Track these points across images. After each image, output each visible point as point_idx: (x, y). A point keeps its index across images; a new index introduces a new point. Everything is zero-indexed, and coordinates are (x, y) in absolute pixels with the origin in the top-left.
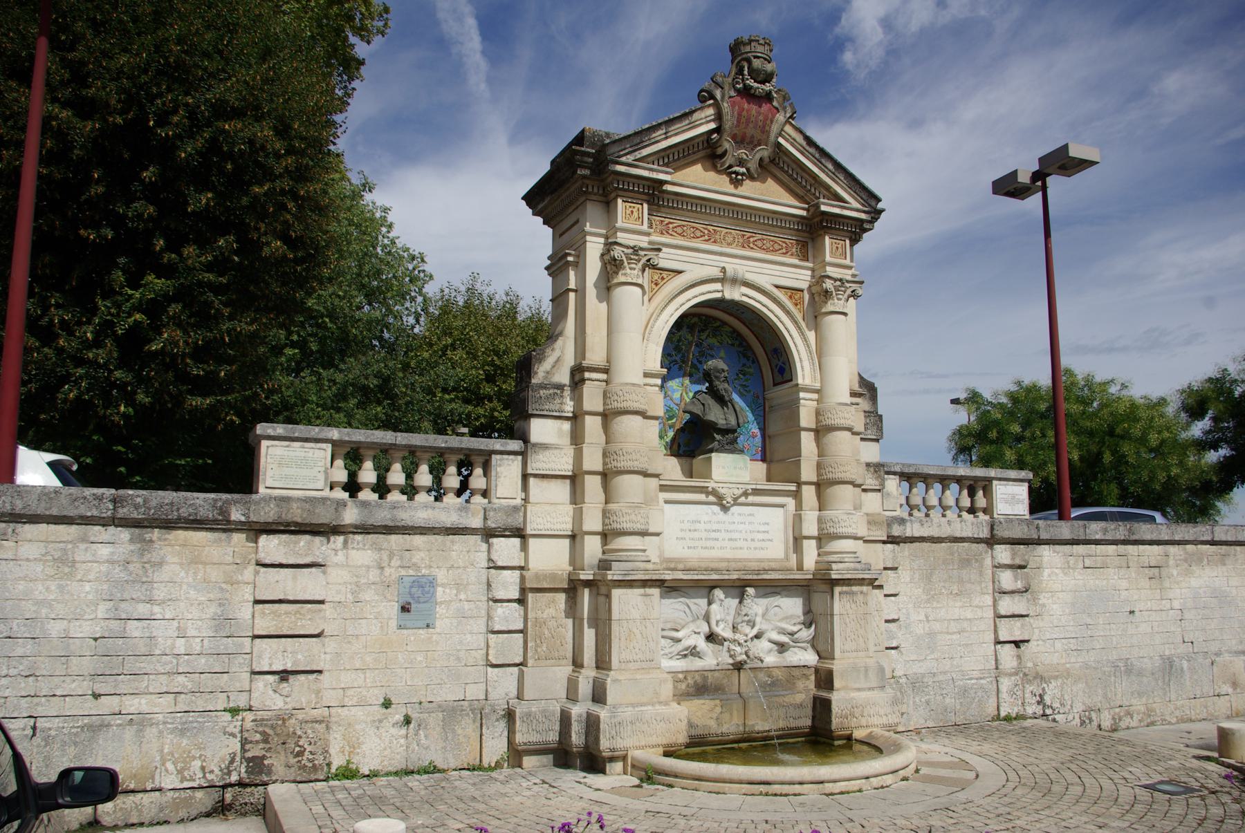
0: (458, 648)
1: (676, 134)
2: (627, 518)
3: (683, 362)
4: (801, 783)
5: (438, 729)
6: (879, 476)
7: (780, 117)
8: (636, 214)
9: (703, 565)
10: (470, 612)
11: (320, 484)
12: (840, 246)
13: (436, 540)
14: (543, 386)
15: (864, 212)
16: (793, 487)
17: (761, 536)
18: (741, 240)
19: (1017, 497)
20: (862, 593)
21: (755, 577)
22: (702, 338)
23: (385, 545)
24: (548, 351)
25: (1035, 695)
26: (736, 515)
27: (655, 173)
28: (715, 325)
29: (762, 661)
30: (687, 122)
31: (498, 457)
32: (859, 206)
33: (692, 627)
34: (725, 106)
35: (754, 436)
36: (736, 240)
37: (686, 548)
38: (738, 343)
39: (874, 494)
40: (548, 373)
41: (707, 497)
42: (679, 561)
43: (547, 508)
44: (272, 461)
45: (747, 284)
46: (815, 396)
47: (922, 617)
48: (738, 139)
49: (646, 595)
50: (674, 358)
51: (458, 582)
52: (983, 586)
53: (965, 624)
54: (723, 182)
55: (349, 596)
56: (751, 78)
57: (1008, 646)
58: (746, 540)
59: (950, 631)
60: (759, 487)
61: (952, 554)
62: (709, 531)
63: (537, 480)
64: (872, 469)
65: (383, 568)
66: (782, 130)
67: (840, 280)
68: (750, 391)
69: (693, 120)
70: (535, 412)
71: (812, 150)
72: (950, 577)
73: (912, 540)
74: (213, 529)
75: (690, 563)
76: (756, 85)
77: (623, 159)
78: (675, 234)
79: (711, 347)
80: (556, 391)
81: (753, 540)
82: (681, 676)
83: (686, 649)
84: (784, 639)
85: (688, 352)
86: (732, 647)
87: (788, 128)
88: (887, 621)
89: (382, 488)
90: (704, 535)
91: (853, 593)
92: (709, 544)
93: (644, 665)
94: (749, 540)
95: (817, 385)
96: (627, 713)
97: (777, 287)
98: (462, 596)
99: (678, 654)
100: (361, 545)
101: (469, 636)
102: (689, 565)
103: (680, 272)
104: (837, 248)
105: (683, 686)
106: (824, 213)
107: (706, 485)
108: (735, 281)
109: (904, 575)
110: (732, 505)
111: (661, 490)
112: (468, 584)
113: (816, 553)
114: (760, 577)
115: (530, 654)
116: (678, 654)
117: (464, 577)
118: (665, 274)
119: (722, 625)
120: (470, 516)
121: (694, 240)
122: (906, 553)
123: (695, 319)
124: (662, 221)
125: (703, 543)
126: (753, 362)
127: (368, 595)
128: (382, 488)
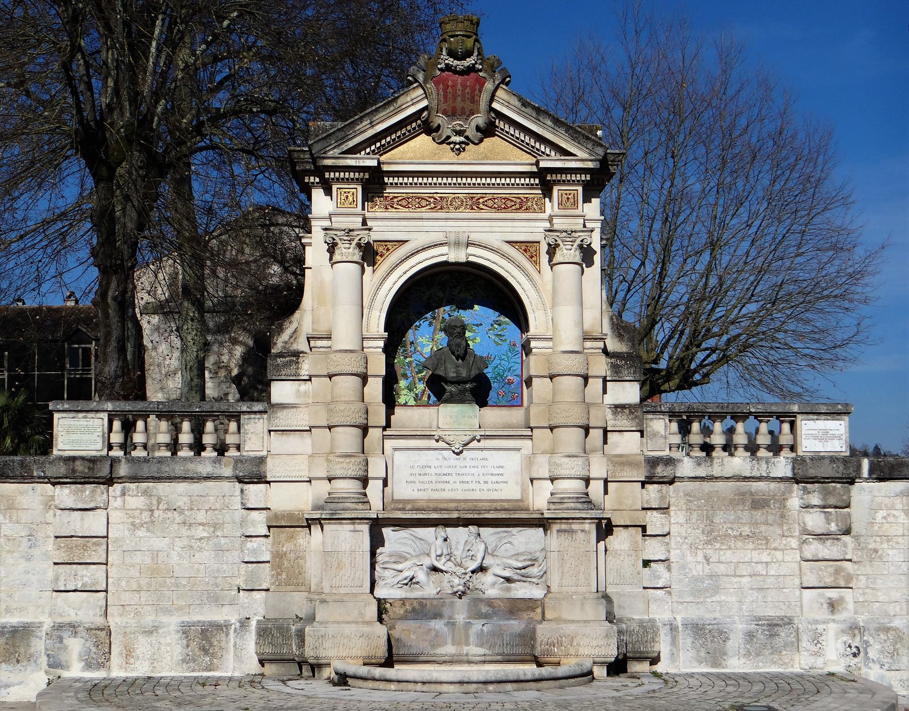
0: (216, 575)
1: (382, 121)
4: (424, 683)
7: (489, 86)
8: (350, 199)
9: (432, 505)
11: (99, 446)
14: (280, 355)
17: (494, 479)
18: (470, 203)
19: (831, 432)
20: (582, 531)
21: (476, 516)
22: (454, 293)
24: (286, 324)
25: (850, 647)
26: (468, 459)
30: (392, 108)
31: (246, 417)
33: (415, 561)
35: (510, 383)
36: (465, 203)
37: (416, 490)
40: (286, 343)
44: (62, 429)
47: (700, 558)
48: (450, 113)
52: (785, 528)
58: (479, 482)
62: (440, 475)
65: (152, 511)
68: (506, 340)
70: (274, 378)
71: (529, 110)
72: (740, 518)
74: (435, 510)
75: (418, 504)
76: (456, 62)
77: (330, 153)
78: (400, 207)
80: (292, 358)
81: (486, 482)
84: (507, 573)
90: (434, 479)
91: (572, 531)
93: (354, 590)
94: (482, 482)
96: (331, 629)
100: (135, 493)
102: (418, 505)
104: (568, 199)
105: (402, 612)
109: (677, 516)
112: (223, 523)
113: (854, 510)
118: (389, 245)
119: (443, 560)
120: (223, 466)
121: (419, 210)
125: (434, 486)
128: (707, 448)
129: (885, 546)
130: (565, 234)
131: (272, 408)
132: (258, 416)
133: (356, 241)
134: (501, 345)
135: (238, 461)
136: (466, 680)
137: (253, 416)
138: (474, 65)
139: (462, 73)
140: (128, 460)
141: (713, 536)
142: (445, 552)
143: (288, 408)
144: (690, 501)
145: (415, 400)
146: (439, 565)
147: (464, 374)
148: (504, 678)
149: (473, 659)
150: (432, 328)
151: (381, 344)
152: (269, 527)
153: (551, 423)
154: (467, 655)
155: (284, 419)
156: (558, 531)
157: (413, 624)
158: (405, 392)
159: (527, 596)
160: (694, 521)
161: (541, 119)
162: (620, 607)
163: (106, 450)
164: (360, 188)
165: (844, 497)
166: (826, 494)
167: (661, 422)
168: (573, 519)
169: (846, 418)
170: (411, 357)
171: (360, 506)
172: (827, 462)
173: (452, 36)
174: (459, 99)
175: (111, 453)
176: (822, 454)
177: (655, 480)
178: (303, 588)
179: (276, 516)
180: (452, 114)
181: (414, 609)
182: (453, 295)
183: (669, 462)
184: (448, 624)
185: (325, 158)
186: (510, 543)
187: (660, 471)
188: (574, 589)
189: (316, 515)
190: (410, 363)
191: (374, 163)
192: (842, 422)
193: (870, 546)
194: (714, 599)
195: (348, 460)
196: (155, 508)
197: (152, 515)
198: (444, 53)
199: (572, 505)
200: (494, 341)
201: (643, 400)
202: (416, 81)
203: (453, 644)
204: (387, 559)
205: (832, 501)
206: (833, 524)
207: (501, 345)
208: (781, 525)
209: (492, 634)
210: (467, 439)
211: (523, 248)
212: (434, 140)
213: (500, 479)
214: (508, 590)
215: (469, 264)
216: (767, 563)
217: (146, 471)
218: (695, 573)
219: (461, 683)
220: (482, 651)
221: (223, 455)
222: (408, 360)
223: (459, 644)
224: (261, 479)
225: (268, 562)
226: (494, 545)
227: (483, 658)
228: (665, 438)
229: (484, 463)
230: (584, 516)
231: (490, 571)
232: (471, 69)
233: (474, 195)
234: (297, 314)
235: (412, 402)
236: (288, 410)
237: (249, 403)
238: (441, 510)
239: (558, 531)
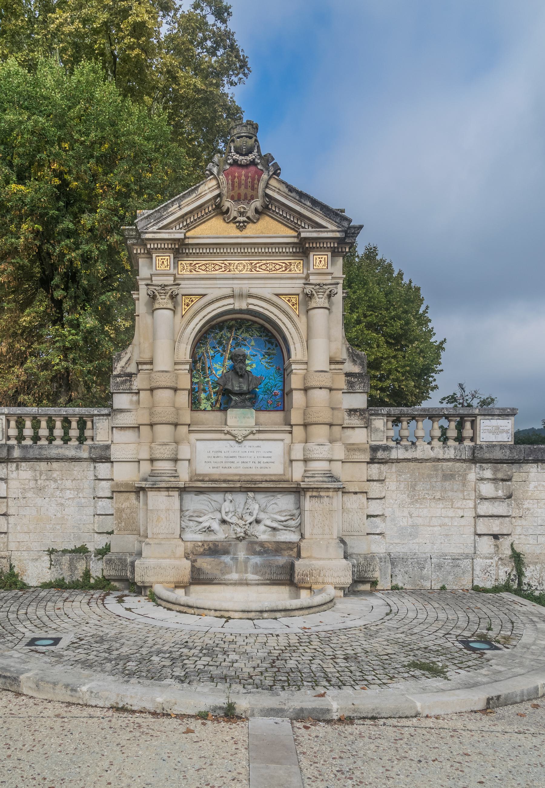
2: (158, 451)
3: (224, 351)
5: (67, 565)
6: (365, 418)
7: (265, 176)
8: (165, 263)
9: (222, 478)
15: (338, 231)
17: (265, 460)
18: (249, 267)
19: (501, 428)
20: (328, 497)
23: (38, 468)
26: (247, 447)
30: (194, 195)
31: (97, 418)
32: (335, 228)
33: (211, 515)
35: (276, 395)
40: (123, 367)
42: (206, 475)
43: (123, 446)
45: (250, 296)
47: (406, 513)
48: (236, 198)
52: (465, 494)
53: (446, 520)
54: (231, 230)
55: (20, 494)
57: (486, 538)
59: (431, 524)
61: (436, 470)
62: (227, 457)
64: (358, 413)
65: (36, 480)
71: (294, 194)
73: (398, 461)
74: (225, 481)
76: (241, 158)
77: (150, 230)
79: (244, 339)
82: (200, 544)
83: (204, 528)
84: (275, 525)
85: (227, 344)
86: (236, 528)
87: (273, 182)
89: (66, 439)
90: (224, 460)
91: (321, 497)
92: (227, 465)
93: (169, 536)
94: (257, 462)
95: (305, 359)
97: (277, 295)
98: (81, 495)
101: (85, 517)
104: (320, 261)
105: (202, 550)
106: (306, 239)
109: (391, 484)
112: (83, 489)
114: (256, 486)
117: (81, 485)
119: (230, 515)
122: (394, 470)
123: (233, 322)
125: (223, 465)
126: (276, 346)
127: (29, 495)
129: (536, 506)
130: (318, 287)
131: (114, 412)
132: (105, 418)
133: (169, 293)
135: (91, 448)
136: (247, 609)
137: (101, 417)
138: (254, 159)
139: (246, 166)
140: (19, 446)
141: (415, 500)
142: (232, 509)
143: (124, 412)
144: (400, 475)
146: (227, 518)
147: (245, 388)
148: (275, 608)
149: (250, 582)
151: (188, 367)
152: (113, 492)
153: (306, 421)
154: (246, 580)
155: (123, 419)
156: (310, 497)
157: (209, 559)
158: (205, 401)
159: (288, 540)
160: (402, 488)
161: (303, 201)
162: (351, 547)
163: (4, 440)
164: (172, 255)
165: (509, 473)
166: (496, 471)
167: (381, 421)
168: (321, 488)
169: (512, 418)
171: (172, 479)
172: (498, 448)
173: (238, 138)
174: (243, 187)
175: (9, 442)
176: (494, 443)
177: (376, 461)
178: (135, 532)
179: (117, 484)
180: (237, 199)
181: (210, 548)
183: (386, 448)
184: (232, 559)
185: (146, 233)
186: (276, 504)
187: (380, 455)
188: (321, 536)
189: (143, 484)
190: (208, 381)
191: (182, 236)
192: (509, 421)
193: (525, 507)
194: (415, 541)
195: (164, 447)
197: (36, 483)
198: (232, 151)
199: (321, 479)
201: (368, 407)
202: (212, 174)
203: (237, 572)
204: (191, 514)
205: (500, 475)
206: (500, 492)
208: (463, 491)
209: (263, 566)
212: (224, 220)
214: (274, 536)
215: (249, 312)
216: (451, 517)
217: (31, 454)
218: (401, 524)
219: (243, 611)
220: (256, 577)
221: (83, 443)
222: (207, 379)
223: (241, 572)
224: (107, 460)
225: (112, 515)
226: (265, 505)
227: (257, 582)
228: (384, 432)
229: (258, 449)
230: (329, 486)
231: (263, 523)
232: (253, 163)
234: (130, 348)
235: (209, 408)
236: (124, 414)
237: (98, 409)
238: (229, 481)
239: (310, 497)
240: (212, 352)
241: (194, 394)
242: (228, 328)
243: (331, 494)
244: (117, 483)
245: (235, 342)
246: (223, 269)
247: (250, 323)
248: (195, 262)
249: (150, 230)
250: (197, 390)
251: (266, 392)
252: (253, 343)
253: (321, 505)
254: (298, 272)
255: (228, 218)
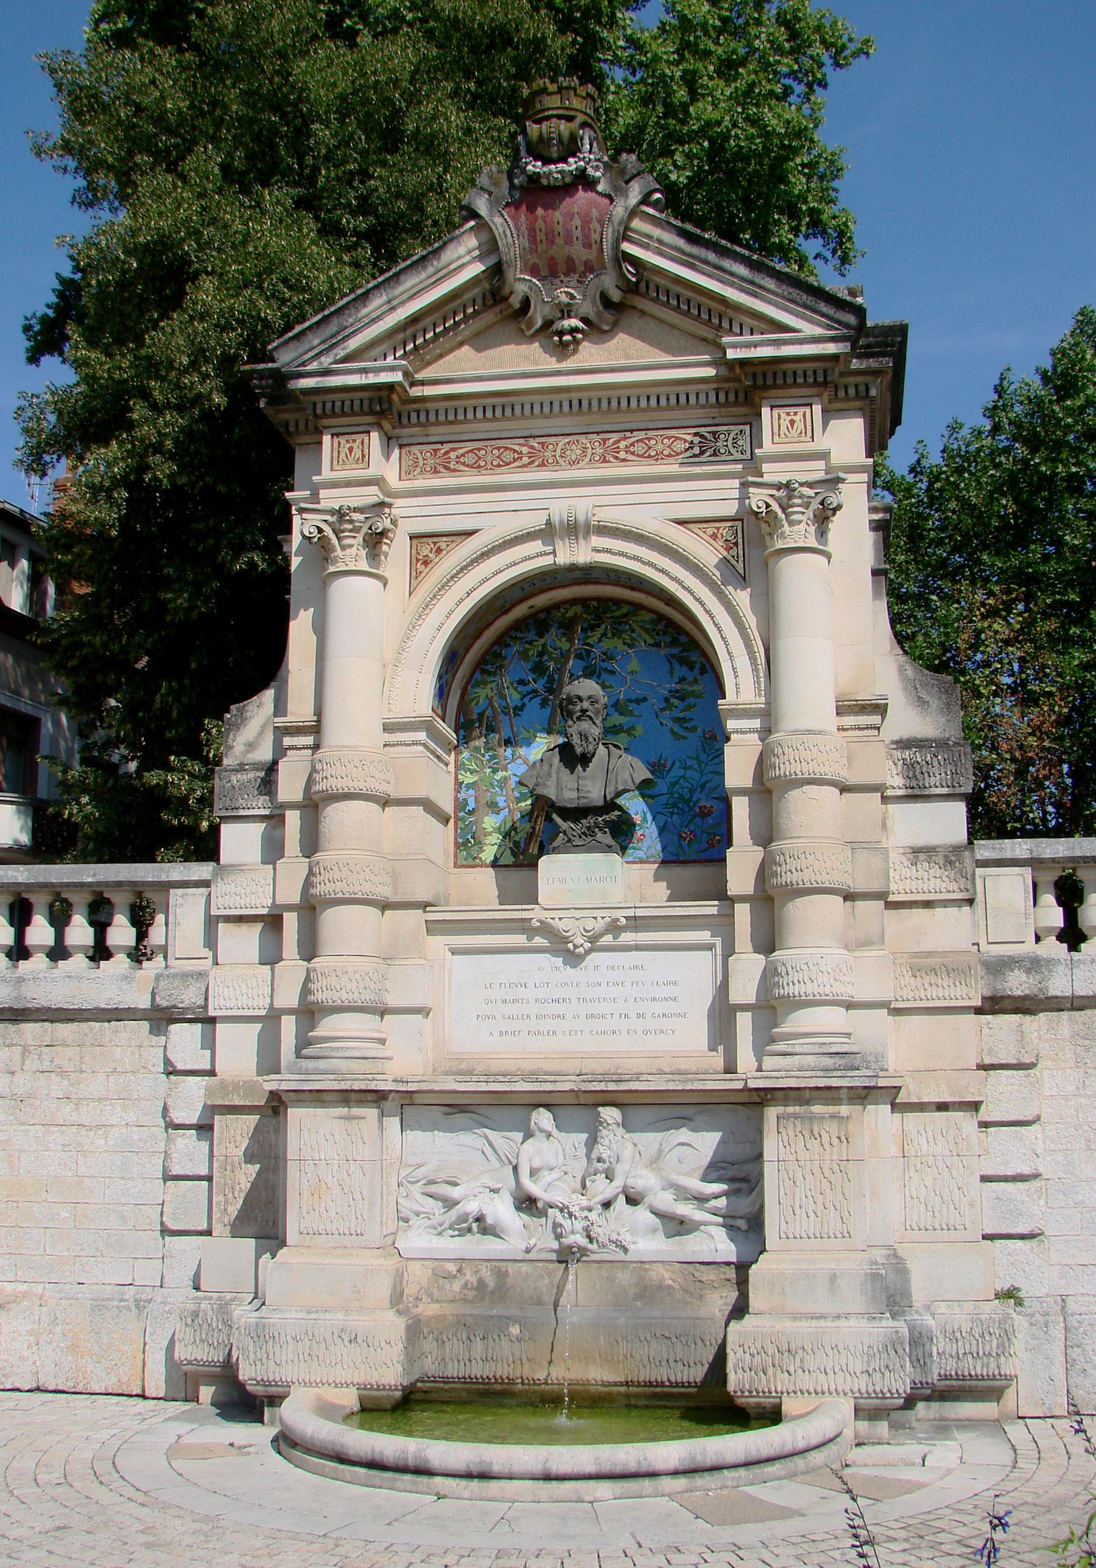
1: (411, 298)
8: (799, 425)
10: (141, 1144)
12: (799, 417)
13: (91, 1029)
16: (711, 908)
17: (659, 1008)
20: (833, 1116)
22: (590, 641)
27: (371, 375)
28: (618, 614)
29: (626, 1250)
30: (431, 270)
31: (180, 891)
32: (819, 331)
34: (498, 223)
37: (496, 1033)
38: (668, 639)
39: (953, 911)
41: (529, 939)
46: (756, 723)
48: (544, 272)
49: (350, 1118)
50: (533, 686)
51: (125, 1095)
56: (536, 160)
58: (626, 1016)
60: (640, 913)
63: (230, 926)
66: (627, 228)
67: (787, 485)
69: (440, 266)
79: (608, 656)
82: (452, 1267)
84: (685, 1209)
88: (985, 1179)
91: (812, 1118)
92: (545, 1025)
94: (632, 1015)
97: (682, 522)
99: (451, 1227)
103: (470, 534)
104: (792, 422)
105: (457, 1286)
107: (526, 915)
108: (573, 530)
110: (588, 952)
111: (429, 932)
114: (623, 1087)
115: (216, 1215)
116: (451, 1227)
118: (442, 543)
119: (547, 1177)
121: (499, 470)
123: (578, 609)
124: (435, 451)
126: (703, 671)
134: (685, 738)
145: (514, 854)
150: (547, 711)
170: (506, 769)
179: (223, 1085)
181: (482, 1283)
182: (588, 644)
190: (505, 779)
196: (18, 1068)
200: (672, 731)
207: (685, 738)
210: (599, 925)
211: (710, 532)
213: (670, 1007)
222: (500, 775)
233: (608, 436)
240: (516, 696)
241: (462, 819)
242: (561, 625)
243: (844, 1110)
244: (223, 1082)
245: (583, 664)
246: (525, 460)
247: (625, 609)
248: (447, 447)
249: (313, 366)
250: (471, 805)
251: (674, 805)
252: (634, 665)
253: (814, 1144)
254: (739, 456)
255: (530, 326)
